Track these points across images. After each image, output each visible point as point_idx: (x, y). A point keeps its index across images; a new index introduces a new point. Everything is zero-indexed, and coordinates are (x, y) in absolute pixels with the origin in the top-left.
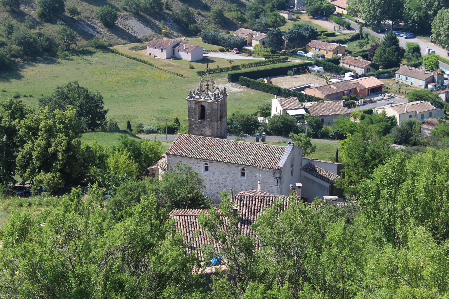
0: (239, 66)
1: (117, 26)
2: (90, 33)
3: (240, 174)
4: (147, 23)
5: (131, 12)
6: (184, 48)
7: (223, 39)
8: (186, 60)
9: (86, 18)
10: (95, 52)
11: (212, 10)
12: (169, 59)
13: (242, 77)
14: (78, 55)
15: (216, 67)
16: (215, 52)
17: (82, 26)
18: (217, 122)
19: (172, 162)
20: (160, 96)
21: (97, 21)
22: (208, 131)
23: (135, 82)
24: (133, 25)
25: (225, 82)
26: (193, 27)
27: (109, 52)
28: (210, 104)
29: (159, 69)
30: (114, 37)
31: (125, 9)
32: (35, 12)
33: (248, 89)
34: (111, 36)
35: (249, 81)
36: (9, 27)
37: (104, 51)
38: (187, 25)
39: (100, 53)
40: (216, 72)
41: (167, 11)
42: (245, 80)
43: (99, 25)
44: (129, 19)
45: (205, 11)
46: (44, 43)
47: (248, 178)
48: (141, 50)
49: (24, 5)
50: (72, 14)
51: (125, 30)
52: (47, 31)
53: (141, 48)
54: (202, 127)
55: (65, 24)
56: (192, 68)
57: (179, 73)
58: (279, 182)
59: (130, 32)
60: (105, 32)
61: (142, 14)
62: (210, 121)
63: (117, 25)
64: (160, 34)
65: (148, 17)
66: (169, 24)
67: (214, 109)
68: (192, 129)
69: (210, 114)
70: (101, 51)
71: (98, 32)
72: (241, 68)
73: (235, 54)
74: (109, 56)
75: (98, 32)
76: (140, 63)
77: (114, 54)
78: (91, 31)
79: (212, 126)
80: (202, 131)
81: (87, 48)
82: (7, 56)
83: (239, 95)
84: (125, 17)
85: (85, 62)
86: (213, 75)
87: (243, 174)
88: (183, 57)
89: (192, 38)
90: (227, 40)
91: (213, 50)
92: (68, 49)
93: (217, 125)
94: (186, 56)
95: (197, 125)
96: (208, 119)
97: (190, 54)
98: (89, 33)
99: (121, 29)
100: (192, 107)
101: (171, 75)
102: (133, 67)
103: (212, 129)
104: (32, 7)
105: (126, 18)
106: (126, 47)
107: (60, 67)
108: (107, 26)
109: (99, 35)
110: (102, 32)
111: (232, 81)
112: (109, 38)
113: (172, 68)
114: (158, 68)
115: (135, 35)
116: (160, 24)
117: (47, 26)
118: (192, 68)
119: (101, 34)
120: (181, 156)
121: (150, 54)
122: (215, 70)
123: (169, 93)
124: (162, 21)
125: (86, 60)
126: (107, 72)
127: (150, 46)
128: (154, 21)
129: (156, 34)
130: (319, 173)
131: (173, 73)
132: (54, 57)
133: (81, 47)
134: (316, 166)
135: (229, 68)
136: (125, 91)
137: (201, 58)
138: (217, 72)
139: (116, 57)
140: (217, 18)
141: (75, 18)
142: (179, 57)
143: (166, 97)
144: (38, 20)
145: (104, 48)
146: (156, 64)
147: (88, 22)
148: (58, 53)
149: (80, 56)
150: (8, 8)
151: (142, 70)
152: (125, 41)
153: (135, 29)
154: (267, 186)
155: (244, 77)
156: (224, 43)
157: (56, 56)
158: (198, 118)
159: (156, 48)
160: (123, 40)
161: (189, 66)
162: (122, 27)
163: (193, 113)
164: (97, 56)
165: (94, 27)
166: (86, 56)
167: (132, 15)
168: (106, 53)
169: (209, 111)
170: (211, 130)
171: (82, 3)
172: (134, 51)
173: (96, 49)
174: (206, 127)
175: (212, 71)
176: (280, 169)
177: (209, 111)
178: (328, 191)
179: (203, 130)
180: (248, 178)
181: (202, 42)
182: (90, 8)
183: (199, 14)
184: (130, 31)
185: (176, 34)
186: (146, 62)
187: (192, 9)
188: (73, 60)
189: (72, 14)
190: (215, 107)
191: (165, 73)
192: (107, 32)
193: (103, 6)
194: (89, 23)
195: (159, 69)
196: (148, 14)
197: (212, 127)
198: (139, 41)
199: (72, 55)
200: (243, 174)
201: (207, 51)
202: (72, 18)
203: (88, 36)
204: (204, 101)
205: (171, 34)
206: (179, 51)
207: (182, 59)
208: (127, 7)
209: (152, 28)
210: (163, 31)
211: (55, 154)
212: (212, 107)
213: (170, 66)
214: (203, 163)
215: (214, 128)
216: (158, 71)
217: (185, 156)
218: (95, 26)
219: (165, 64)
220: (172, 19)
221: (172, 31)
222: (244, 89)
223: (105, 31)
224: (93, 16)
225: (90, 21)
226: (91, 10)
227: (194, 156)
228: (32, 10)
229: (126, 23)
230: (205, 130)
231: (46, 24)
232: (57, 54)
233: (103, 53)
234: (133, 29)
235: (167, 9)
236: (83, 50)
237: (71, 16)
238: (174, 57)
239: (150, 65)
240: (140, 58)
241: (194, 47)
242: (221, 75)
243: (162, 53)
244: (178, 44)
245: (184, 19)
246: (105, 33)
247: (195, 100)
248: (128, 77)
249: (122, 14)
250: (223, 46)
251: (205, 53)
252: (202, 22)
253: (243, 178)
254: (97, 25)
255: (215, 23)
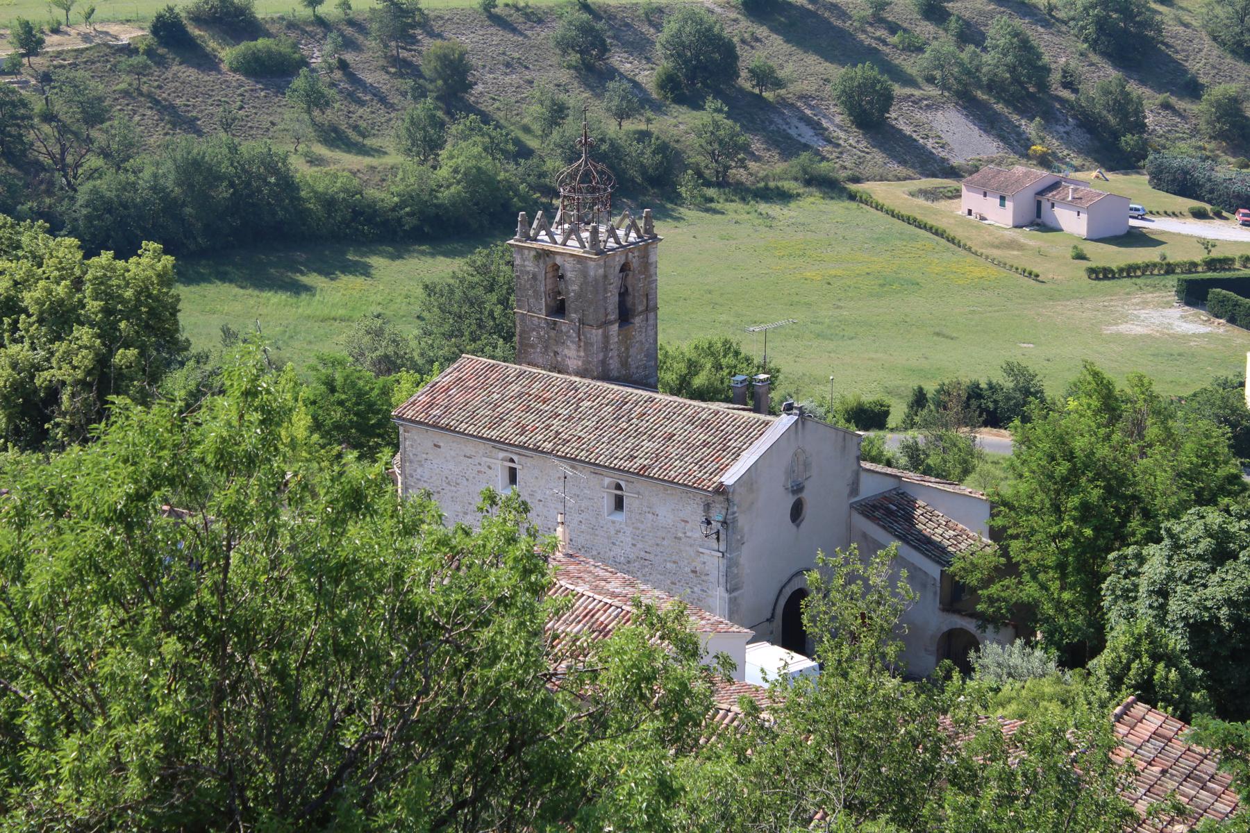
0: (1233, 260)
1: (893, 127)
2: (803, 141)
3: (607, 502)
4: (989, 122)
5: (945, 87)
6: (1070, 198)
7: (1209, 180)
8: (1071, 235)
9: (801, 97)
10: (798, 195)
11: (1205, 97)
12: (1022, 227)
13: (1219, 290)
14: (743, 199)
15: (1158, 260)
16: (1169, 216)
17: (784, 120)
18: (605, 324)
19: (412, 446)
20: (937, 330)
21: (833, 109)
22: (572, 355)
23: (882, 286)
24: (945, 127)
25: (1168, 302)
26: (1132, 143)
27: (840, 197)
28: (579, 262)
29: (975, 253)
30: (878, 156)
31: (930, 80)
32: (652, 74)
33: (1230, 327)
34: (868, 153)
35: (1236, 304)
36: (552, 111)
37: (825, 193)
38: (1116, 136)
39: (812, 199)
40: (1152, 274)
41: (1066, 94)
42: (1223, 302)
43: (838, 119)
44: (936, 109)
45: (1187, 100)
46: (648, 159)
47: (630, 518)
48: (950, 198)
49: (626, 52)
50: (758, 85)
51: (915, 140)
52: (671, 128)
53: (950, 194)
54: (557, 342)
55: (726, 109)
56: (1080, 257)
57: (1028, 270)
58: (722, 537)
59: (929, 146)
60: (851, 141)
61: (980, 94)
62: (579, 320)
63: (894, 123)
64: (1028, 157)
65: (999, 107)
66: (1062, 129)
67: (590, 280)
68: (527, 345)
69: (579, 296)
70: (817, 194)
71: (829, 141)
72: (1237, 265)
73: (1239, 226)
74: (838, 208)
75: (829, 141)
76: (923, 231)
77: (853, 205)
78: (807, 135)
79: (586, 337)
80: (556, 353)
81: (780, 184)
82: (521, 187)
83: (1192, 344)
84: (925, 102)
85: (757, 222)
86: (1138, 281)
87: (619, 504)
88: (1063, 225)
89: (1126, 174)
90: (1222, 184)
91: (1169, 212)
92: (722, 183)
93: (606, 337)
94: (1073, 223)
95: (542, 333)
96: (574, 315)
97: (1084, 216)
98: (800, 142)
99: (905, 135)
100: (528, 269)
101: (1003, 273)
102: (898, 243)
103: (585, 350)
104: (648, 60)
105: (927, 105)
106: (903, 186)
107: (677, 230)
108: (859, 126)
109: (829, 148)
110: (841, 142)
111: (1188, 303)
112: (860, 158)
113: (1015, 253)
114: (973, 250)
115: (943, 154)
116: (1030, 128)
117: (676, 114)
118: (1080, 257)
119: (838, 145)
120: (435, 426)
121: (970, 212)
122: (1147, 266)
123: (973, 323)
124: (1038, 119)
125: (761, 214)
126: (808, 253)
127: (970, 187)
128: (1015, 118)
129: (1012, 156)
130: (920, 526)
131: (1012, 266)
132: (672, 202)
133: (765, 179)
134: (920, 503)
135: (1195, 265)
136: (838, 307)
137: (1121, 231)
138: (1156, 272)
139: (858, 212)
140: (1218, 120)
141: (768, 95)
142: (1052, 225)
143: (954, 335)
144: (654, 96)
145: (830, 186)
146: (971, 240)
147: (806, 111)
148: (684, 189)
149: (748, 204)
150: (574, 58)
151: (921, 252)
152: (902, 170)
153: (946, 138)
154: (688, 548)
155: (1224, 292)
156: (1211, 191)
157: (676, 199)
158: (544, 311)
159: (985, 195)
160: (901, 168)
161: (1071, 250)
162: (908, 130)
163: (530, 292)
164: (799, 207)
165: (819, 124)
166: (767, 205)
167: (948, 98)
168: (832, 198)
169: (575, 288)
170: (582, 354)
171: (804, 56)
172: (921, 201)
173: (805, 186)
174: (569, 343)
175: (1139, 268)
176: (721, 490)
177: (575, 288)
178: (935, 593)
179: (559, 350)
180: (630, 518)
181: (1150, 187)
182: (822, 70)
183: (1166, 106)
184: (930, 144)
185: (1077, 162)
186: (939, 231)
187: (1135, 89)
188: (723, 213)
189: (758, 85)
190: (592, 273)
191: (990, 265)
192: (858, 142)
193: (855, 65)
194: (808, 112)
195: (975, 253)
196: (999, 98)
197: (586, 344)
198: (953, 172)
199: (726, 200)
200: (619, 504)
201: (1151, 212)
202: (760, 97)
203: (788, 147)
204: (559, 249)
205: (1062, 160)
206: (1053, 206)
207: (1061, 230)
208: (938, 74)
209: (1002, 138)
210: (1034, 147)
211: (53, 393)
212: (584, 274)
213: (1013, 249)
214: (502, 455)
215: (592, 345)
216: (971, 258)
217: (447, 429)
218: (825, 123)
219: (997, 242)
220: (1074, 117)
221: (1065, 152)
222: (1220, 327)
223: (852, 140)
224: (825, 94)
225: (812, 108)
226: (825, 77)
227: (471, 430)
228: (647, 67)
229: (925, 120)
230: (566, 351)
231: (676, 109)
232: (679, 195)
233: (823, 198)
234: (940, 137)
235: (1067, 85)
236: (767, 188)
237: (757, 91)
238: (1038, 225)
239: (952, 240)
240: (930, 221)
241: (1099, 195)
242: (1162, 284)
243: (1001, 210)
244: (1055, 186)
245: (1110, 117)
246: (850, 145)
247: (535, 245)
248: (868, 270)
249: (917, 93)
250: (1209, 202)
251: (1143, 219)
252: (1169, 131)
253: (619, 517)
254: (831, 121)
255: (1210, 138)
